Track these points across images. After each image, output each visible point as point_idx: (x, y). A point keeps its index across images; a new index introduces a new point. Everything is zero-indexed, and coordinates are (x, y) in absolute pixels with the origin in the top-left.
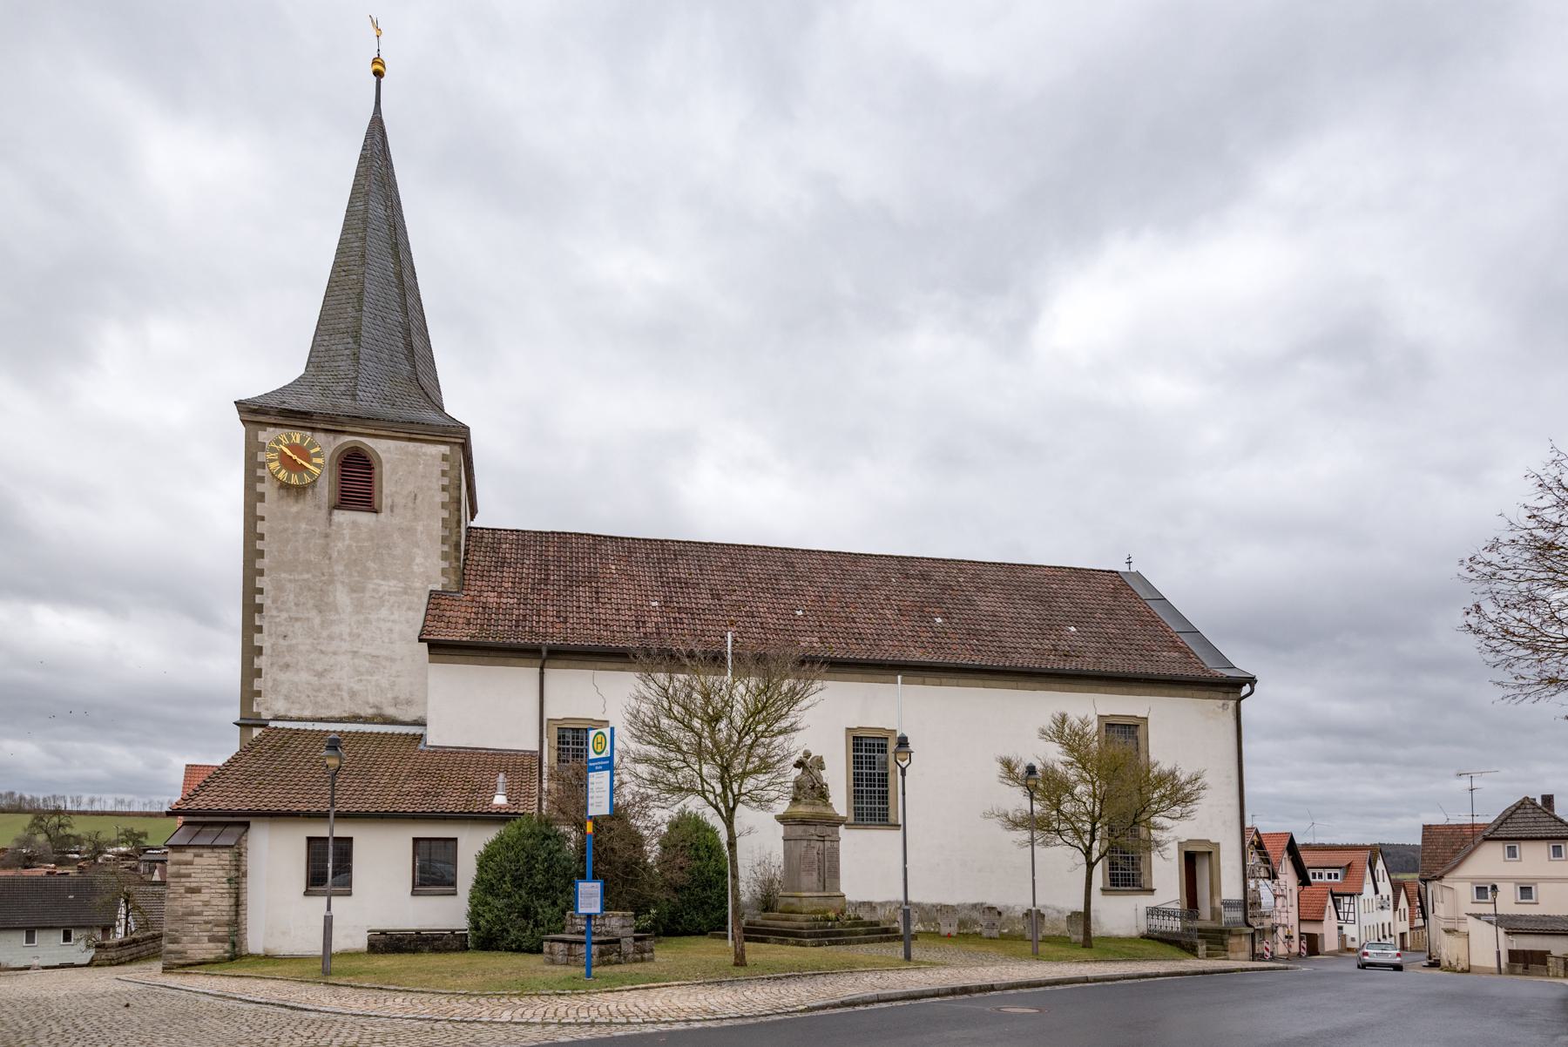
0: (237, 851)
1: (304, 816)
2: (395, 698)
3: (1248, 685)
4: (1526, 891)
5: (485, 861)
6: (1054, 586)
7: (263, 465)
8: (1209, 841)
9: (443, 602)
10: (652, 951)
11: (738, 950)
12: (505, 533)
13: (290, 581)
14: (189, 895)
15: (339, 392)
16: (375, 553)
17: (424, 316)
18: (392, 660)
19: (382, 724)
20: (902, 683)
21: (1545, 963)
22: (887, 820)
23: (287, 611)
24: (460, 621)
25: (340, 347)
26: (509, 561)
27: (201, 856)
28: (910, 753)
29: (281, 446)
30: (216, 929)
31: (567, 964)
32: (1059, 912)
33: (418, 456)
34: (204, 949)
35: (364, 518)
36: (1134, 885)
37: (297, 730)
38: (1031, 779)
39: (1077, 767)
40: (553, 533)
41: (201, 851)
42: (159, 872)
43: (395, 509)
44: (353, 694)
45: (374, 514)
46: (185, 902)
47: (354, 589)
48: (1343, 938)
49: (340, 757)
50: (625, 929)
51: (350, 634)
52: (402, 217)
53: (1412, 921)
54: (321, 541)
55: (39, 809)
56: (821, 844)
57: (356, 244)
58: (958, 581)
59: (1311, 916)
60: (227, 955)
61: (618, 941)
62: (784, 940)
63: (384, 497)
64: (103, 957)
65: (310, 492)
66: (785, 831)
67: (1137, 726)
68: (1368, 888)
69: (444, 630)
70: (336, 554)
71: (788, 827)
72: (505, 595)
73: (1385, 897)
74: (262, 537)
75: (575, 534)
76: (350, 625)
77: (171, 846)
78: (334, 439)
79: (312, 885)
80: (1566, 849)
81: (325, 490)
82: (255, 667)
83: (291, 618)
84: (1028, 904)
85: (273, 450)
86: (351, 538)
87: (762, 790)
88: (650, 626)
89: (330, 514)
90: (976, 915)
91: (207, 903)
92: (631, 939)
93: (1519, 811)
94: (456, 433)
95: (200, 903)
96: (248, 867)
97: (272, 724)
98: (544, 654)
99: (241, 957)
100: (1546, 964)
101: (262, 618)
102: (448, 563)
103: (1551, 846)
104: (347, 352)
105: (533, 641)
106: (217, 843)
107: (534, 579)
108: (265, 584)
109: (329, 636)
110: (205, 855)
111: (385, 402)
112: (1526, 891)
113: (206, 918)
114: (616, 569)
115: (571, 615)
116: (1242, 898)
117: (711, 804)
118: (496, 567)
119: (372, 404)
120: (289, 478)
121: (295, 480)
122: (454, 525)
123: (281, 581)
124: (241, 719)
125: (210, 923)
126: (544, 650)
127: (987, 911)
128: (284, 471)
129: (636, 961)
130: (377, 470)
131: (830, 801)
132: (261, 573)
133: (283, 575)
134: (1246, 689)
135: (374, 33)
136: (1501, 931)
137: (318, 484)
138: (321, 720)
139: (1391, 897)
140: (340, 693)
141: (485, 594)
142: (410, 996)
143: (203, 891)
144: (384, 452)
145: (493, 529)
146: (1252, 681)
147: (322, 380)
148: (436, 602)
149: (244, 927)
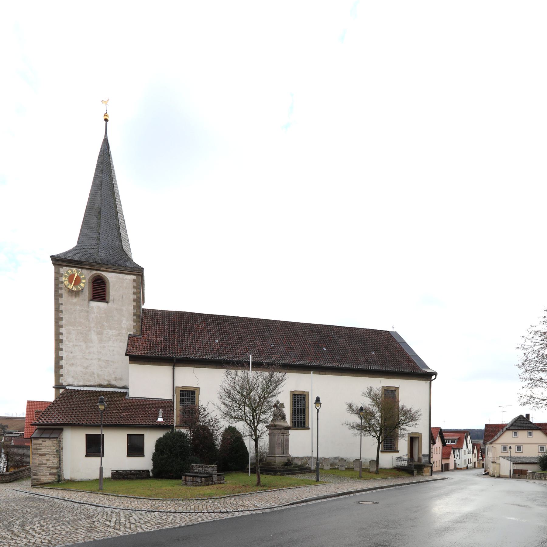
2: (115, 378)
3: (434, 375)
4: (519, 448)
6: (367, 336)
7: (62, 282)
8: (418, 433)
14: (41, 457)
16: (107, 319)
17: (125, 222)
19: (110, 388)
20: (313, 374)
21: (526, 474)
22: (305, 426)
26: (159, 323)
27: (45, 442)
28: (320, 404)
31: (192, 485)
32: (365, 460)
33: (124, 280)
34: (47, 478)
36: (392, 449)
38: (362, 412)
39: (376, 407)
41: (45, 440)
42: (14, 441)
43: (114, 301)
44: (99, 376)
47: (100, 333)
48: (455, 464)
51: (97, 352)
53: (478, 458)
56: (282, 437)
58: (331, 334)
59: (446, 456)
60: (57, 480)
63: (110, 296)
64: (4, 479)
67: (395, 390)
68: (465, 446)
70: (91, 319)
73: (470, 449)
76: (97, 348)
78: (90, 272)
79: (88, 452)
80: (533, 433)
81: (87, 293)
82: (60, 364)
84: (358, 457)
86: (97, 313)
89: (89, 303)
90: (336, 461)
91: (48, 460)
93: (519, 420)
95: (45, 460)
97: (67, 388)
98: (175, 361)
100: (526, 475)
103: (528, 432)
105: (171, 356)
109: (89, 353)
112: (519, 448)
113: (48, 466)
114: (201, 327)
116: (429, 454)
117: (248, 424)
124: (55, 385)
125: (50, 468)
127: (341, 460)
131: (286, 420)
132: (61, 326)
133: (70, 327)
134: (433, 377)
136: (512, 463)
137: (84, 290)
138: (87, 386)
139: (472, 449)
141: (150, 336)
142: (140, 500)
143: (46, 455)
144: (110, 278)
146: (436, 374)
149: (62, 469)
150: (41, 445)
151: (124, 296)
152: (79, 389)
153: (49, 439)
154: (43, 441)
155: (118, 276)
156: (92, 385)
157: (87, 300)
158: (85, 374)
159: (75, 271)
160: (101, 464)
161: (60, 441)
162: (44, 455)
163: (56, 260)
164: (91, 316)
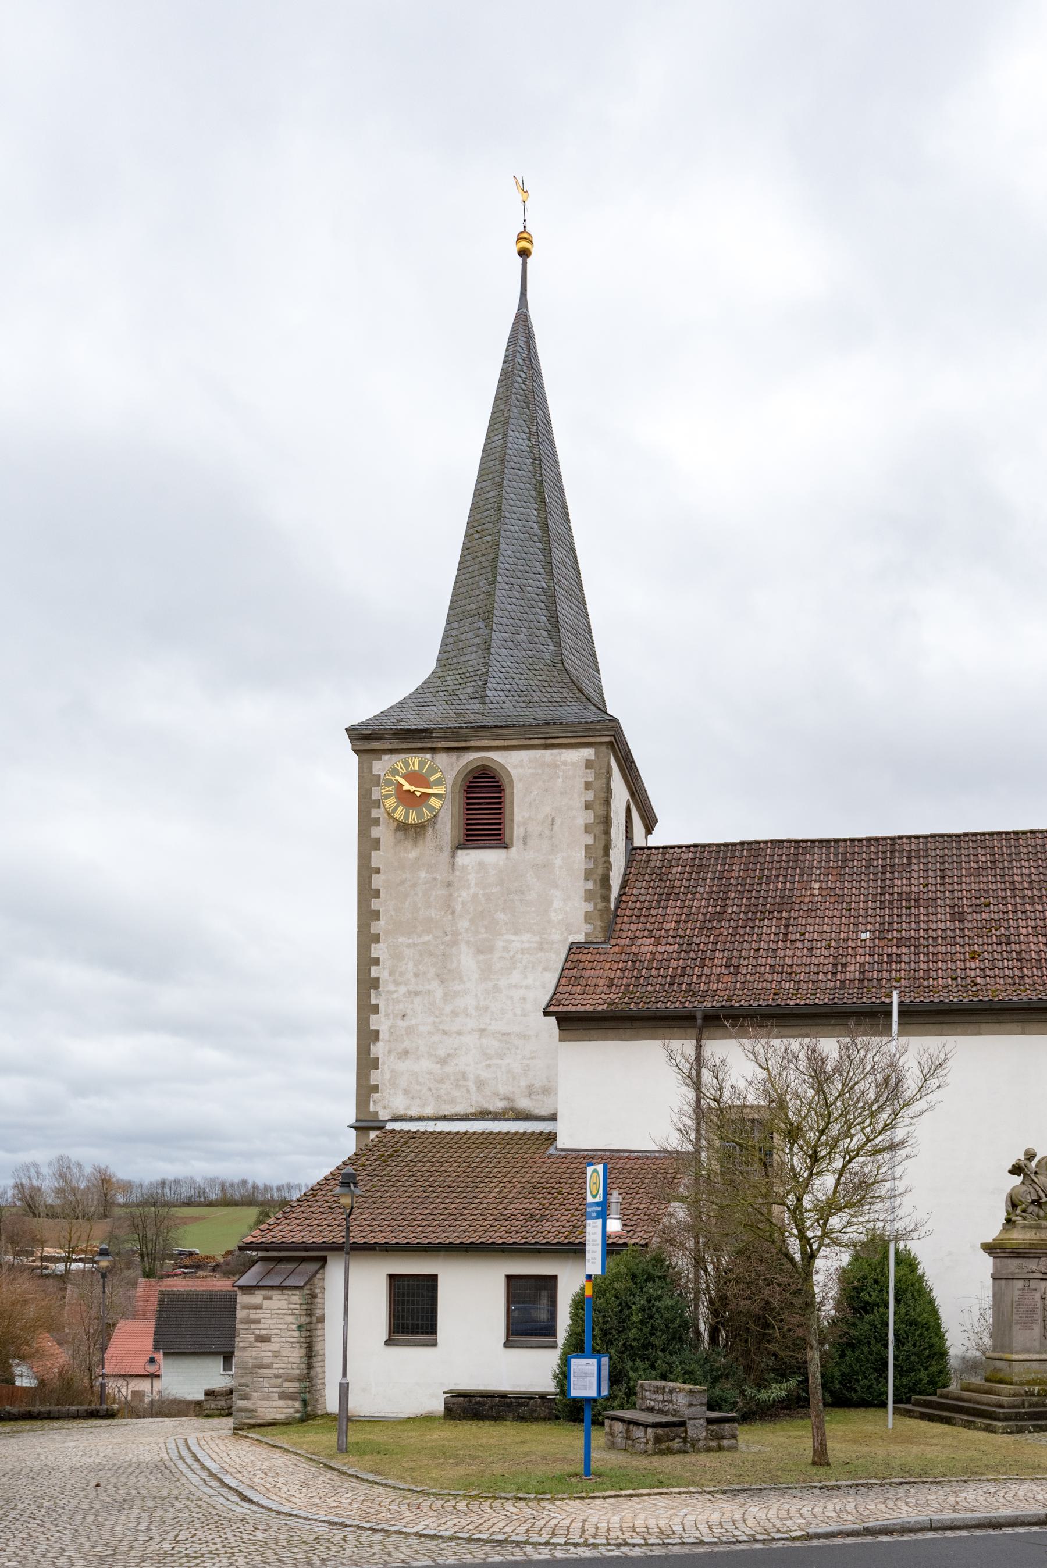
0: (308, 1292)
1: (381, 1250)
2: (530, 1086)
5: (579, 1303)
7: (378, 803)
9: (583, 958)
10: (734, 1437)
11: (816, 1444)
12: (680, 850)
13: (409, 946)
14: (258, 1344)
15: (466, 696)
18: (525, 1037)
23: (406, 985)
24: (601, 982)
25: (469, 635)
27: (270, 1298)
29: (397, 778)
30: (286, 1384)
34: (275, 1408)
35: (490, 857)
37: (416, 1132)
40: (742, 843)
43: (528, 840)
44: (480, 1084)
45: (505, 850)
46: (255, 1352)
47: (483, 949)
49: (353, 1195)
50: (694, 1408)
51: (477, 1008)
52: (552, 443)
54: (443, 892)
55: (273, 1200)
57: (492, 494)
60: (298, 1415)
61: (683, 1424)
62: (972, 1422)
63: (515, 827)
65: (430, 830)
66: (995, 1265)
69: (580, 997)
71: (998, 1260)
72: (664, 941)
74: (377, 894)
75: (772, 841)
76: (476, 996)
77: (240, 1287)
78: (458, 758)
81: (447, 827)
82: (371, 1056)
83: (409, 992)
85: (389, 783)
86: (476, 884)
87: (840, 1232)
88: (852, 972)
89: (453, 856)
92: (703, 1422)
94: (602, 729)
95: (270, 1354)
96: (326, 1310)
97: (390, 1126)
98: (699, 1021)
99: (316, 1417)
101: (378, 994)
102: (592, 905)
104: (478, 640)
106: (287, 1283)
107: (704, 915)
108: (381, 952)
109: (453, 1012)
110: (274, 1298)
111: (519, 700)
113: (276, 1371)
114: (821, 888)
115: (746, 963)
118: (659, 902)
119: (504, 706)
120: (407, 816)
121: (413, 818)
122: (601, 853)
123: (399, 946)
125: (281, 1377)
126: (699, 1015)
128: (401, 808)
129: (709, 1450)
130: (507, 791)
132: (377, 939)
135: (519, 197)
137: (439, 819)
138: (445, 1118)
140: (465, 1083)
143: (273, 1340)
144: (515, 767)
145: (664, 848)
147: (449, 683)
148: (576, 957)
150: (261, 1308)
151: (558, 821)
152: (422, 1129)
153: (280, 1292)
154: (265, 1298)
155: (538, 756)
156: (460, 1115)
157: (449, 849)
158: (441, 1081)
159: (413, 764)
160: (344, 1375)
161: (314, 1296)
162: (264, 1339)
163: (362, 739)
164: (460, 896)
